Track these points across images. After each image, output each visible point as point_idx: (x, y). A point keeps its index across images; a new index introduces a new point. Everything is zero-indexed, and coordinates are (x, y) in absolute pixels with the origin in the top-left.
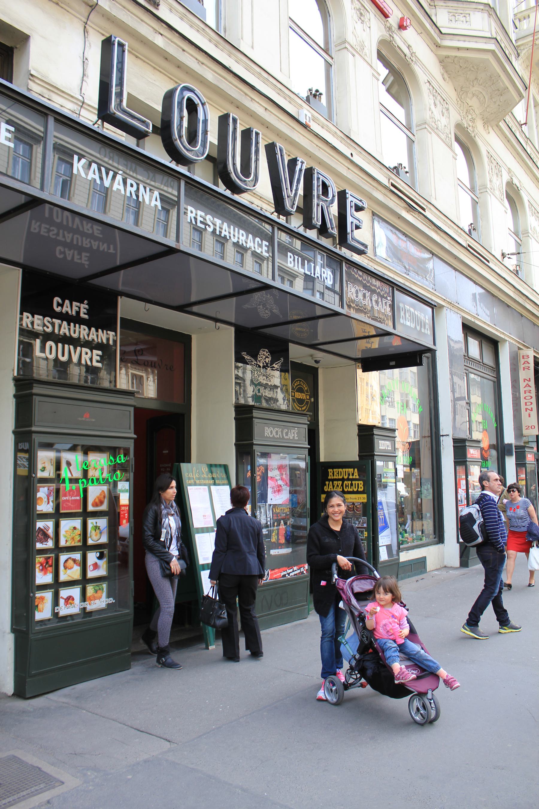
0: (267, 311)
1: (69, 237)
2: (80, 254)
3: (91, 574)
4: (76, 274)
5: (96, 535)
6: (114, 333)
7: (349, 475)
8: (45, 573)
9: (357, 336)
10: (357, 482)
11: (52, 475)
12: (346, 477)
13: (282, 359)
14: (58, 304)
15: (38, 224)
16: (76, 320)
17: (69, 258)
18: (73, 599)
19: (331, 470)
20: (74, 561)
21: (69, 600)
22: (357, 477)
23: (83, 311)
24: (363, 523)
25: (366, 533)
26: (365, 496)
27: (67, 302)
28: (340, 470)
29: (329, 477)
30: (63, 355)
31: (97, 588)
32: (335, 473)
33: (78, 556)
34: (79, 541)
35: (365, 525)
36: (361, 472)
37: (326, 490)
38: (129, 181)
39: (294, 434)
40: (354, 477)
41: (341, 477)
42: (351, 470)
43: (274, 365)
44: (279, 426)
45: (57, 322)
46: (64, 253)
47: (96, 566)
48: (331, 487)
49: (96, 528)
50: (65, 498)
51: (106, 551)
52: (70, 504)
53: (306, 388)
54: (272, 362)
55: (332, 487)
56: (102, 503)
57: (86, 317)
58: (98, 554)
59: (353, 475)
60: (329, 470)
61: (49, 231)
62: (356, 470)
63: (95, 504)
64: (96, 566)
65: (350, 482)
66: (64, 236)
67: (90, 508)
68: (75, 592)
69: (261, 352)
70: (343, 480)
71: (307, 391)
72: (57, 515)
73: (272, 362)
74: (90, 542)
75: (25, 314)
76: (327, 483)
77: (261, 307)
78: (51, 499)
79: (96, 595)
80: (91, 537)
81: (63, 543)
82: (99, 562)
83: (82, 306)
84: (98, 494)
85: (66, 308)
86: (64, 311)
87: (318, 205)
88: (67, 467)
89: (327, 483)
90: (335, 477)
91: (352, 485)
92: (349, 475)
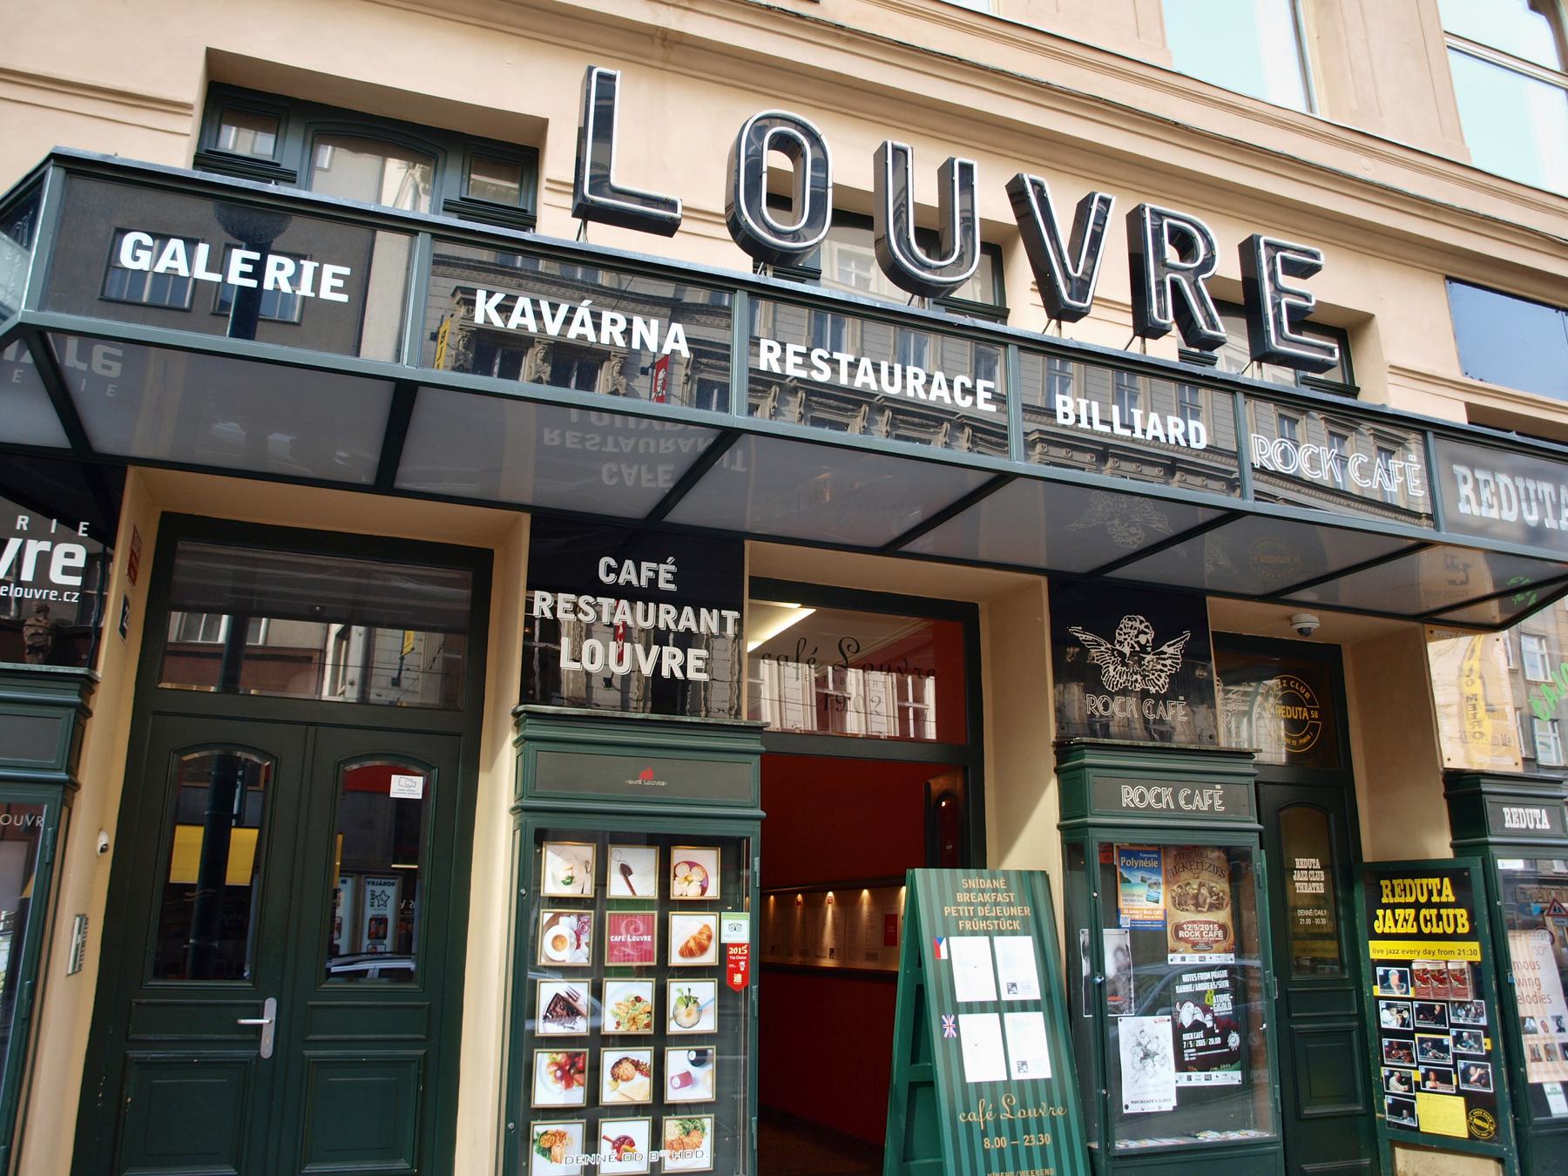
0: (1133, 530)
1: (627, 445)
2: (652, 470)
3: (674, 1095)
4: (637, 508)
5: (689, 1015)
6: (736, 614)
7: (1430, 893)
8: (568, 1086)
9: (1333, 567)
10: (1451, 912)
11: (589, 892)
12: (1423, 899)
13: (1188, 634)
14: (609, 570)
15: (557, 432)
16: (651, 595)
17: (630, 483)
18: (632, 1144)
19: (1387, 882)
20: (637, 1065)
21: (623, 1144)
22: (1452, 899)
23: (663, 576)
24: (1478, 1015)
25: (1488, 1041)
26: (1475, 945)
27: (629, 564)
28: (1408, 882)
29: (1384, 900)
30: (891, 384)
31: (689, 1125)
32: (1397, 890)
33: (645, 1056)
34: (647, 1026)
35: (1483, 1021)
36: (1461, 881)
37: (1379, 931)
38: (607, 316)
39: (1211, 797)
40: (1444, 899)
41: (1412, 900)
42: (1434, 882)
43: (1165, 648)
44: (1163, 783)
45: (606, 603)
46: (619, 473)
47: (686, 1079)
48: (1390, 922)
49: (689, 1000)
50: (617, 939)
51: (711, 1050)
52: (628, 951)
53: (1307, 695)
54: (1158, 642)
55: (1391, 923)
56: (703, 949)
57: (672, 587)
58: (693, 1056)
59: (1440, 893)
60: (1383, 883)
61: (583, 440)
62: (1446, 881)
63: (687, 952)
64: (686, 1079)
65: (1434, 912)
66: (617, 444)
67: (676, 960)
68: (639, 1130)
69: (1125, 621)
70: (1417, 906)
71: (1311, 701)
72: (597, 973)
73: (1158, 642)
74: (673, 1028)
75: (538, 594)
76: (1380, 912)
77: (1117, 522)
78: (585, 939)
79: (686, 1140)
80: (675, 1017)
81: (609, 1027)
82: (694, 1071)
83: (662, 567)
84: (695, 932)
85: (628, 574)
86: (621, 581)
87: (1161, 283)
88: (621, 878)
89: (1380, 912)
90: (1397, 900)
91: (1439, 917)
92: (1430, 893)
